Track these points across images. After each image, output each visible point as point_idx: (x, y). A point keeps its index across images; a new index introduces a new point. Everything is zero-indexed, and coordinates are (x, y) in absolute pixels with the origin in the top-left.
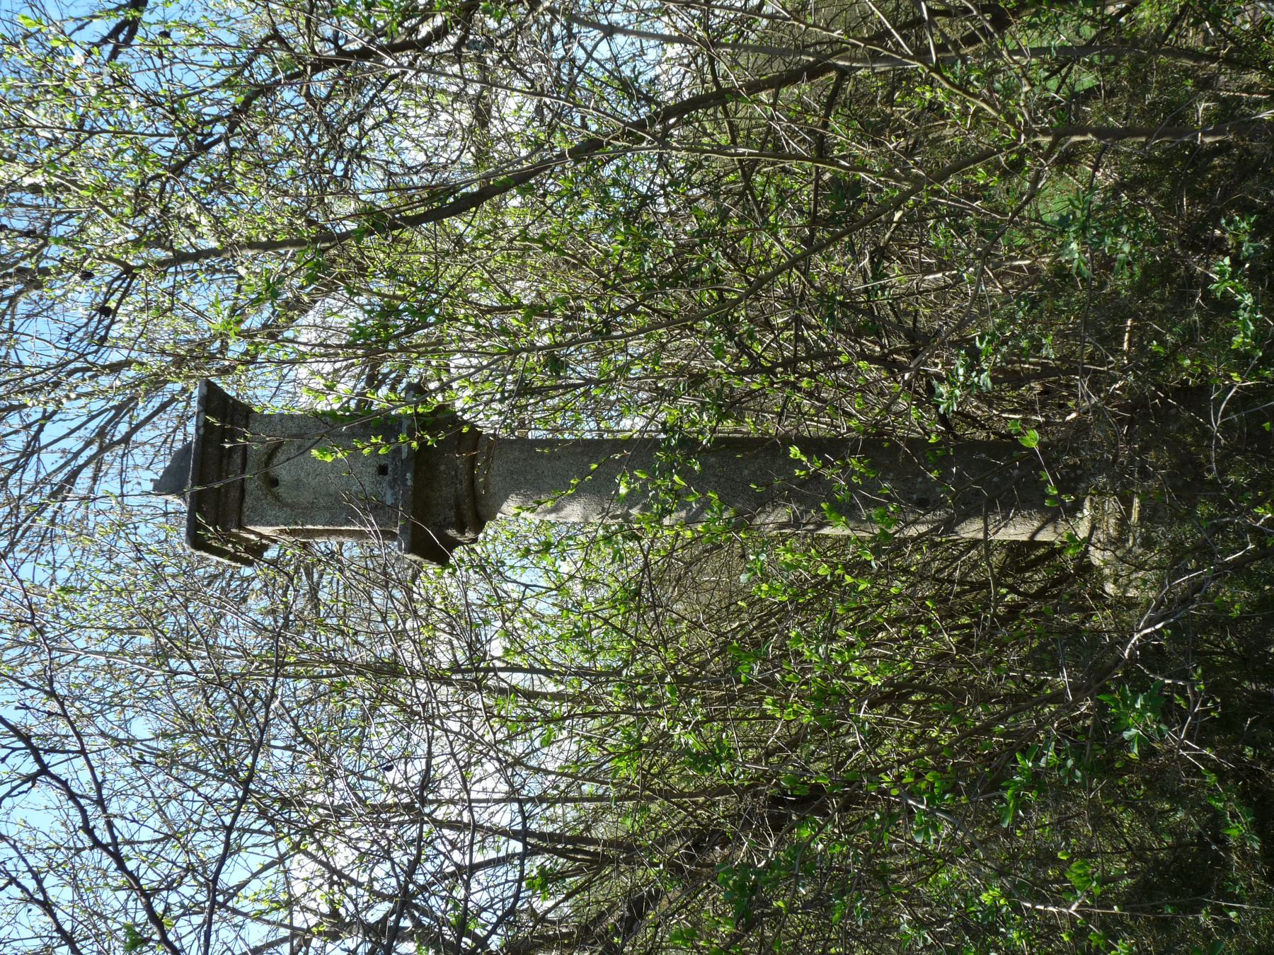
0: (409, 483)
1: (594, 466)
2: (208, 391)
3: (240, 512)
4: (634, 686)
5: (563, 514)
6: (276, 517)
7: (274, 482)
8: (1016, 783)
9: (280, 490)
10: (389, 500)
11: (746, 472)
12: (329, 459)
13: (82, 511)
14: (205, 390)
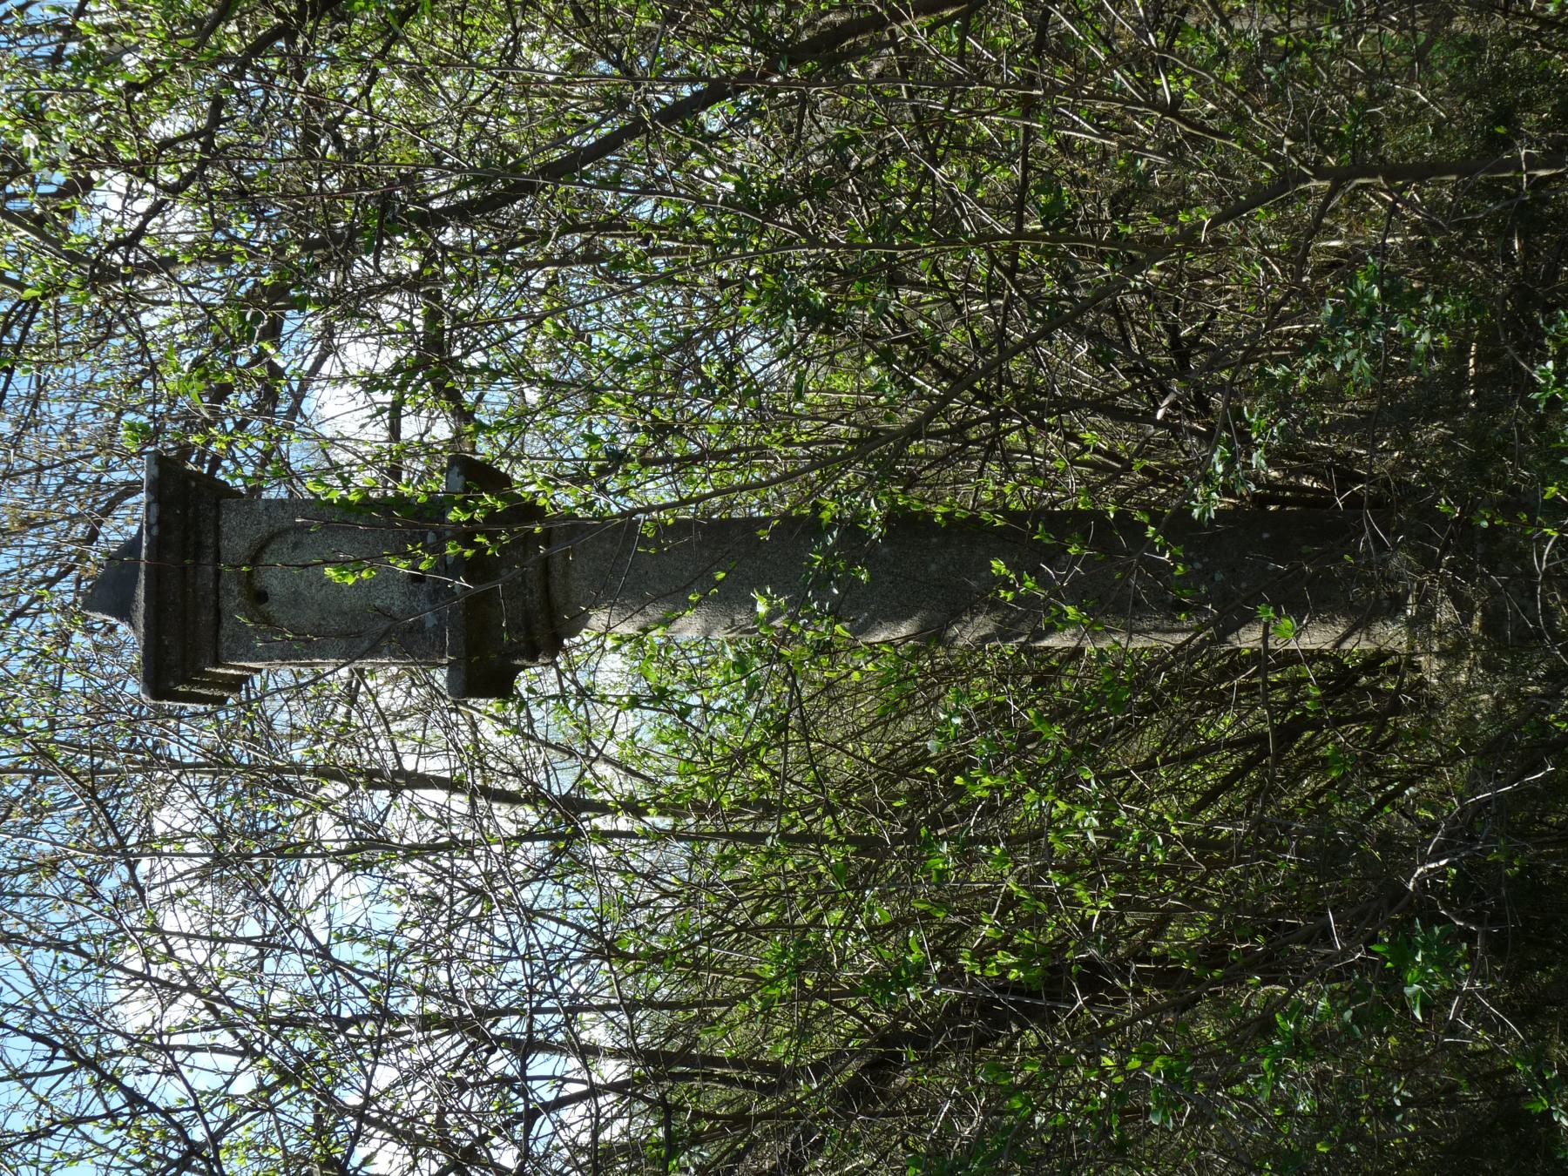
1: (721, 575)
2: (161, 471)
5: (674, 627)
7: (261, 597)
8: (1275, 1049)
9: (271, 608)
10: (430, 620)
11: (933, 567)
12: (350, 581)
13: (283, 1106)
14: (155, 471)
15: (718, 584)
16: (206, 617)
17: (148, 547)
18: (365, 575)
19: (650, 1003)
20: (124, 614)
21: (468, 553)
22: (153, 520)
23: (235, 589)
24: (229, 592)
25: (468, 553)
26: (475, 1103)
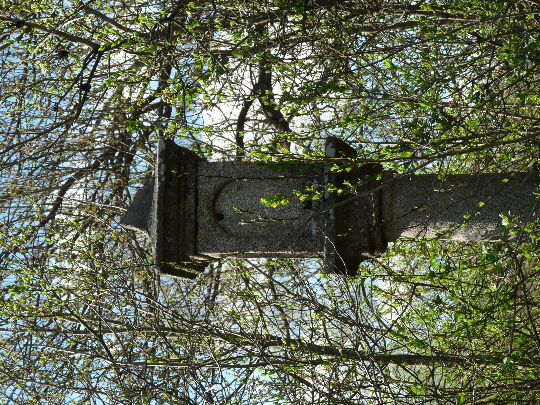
0: (332, 217)
1: (482, 204)
2: (166, 146)
3: (196, 242)
4: (484, 266)
6: (225, 245)
7: (220, 217)
12: (274, 206)
14: (164, 146)
15: (480, 209)
16: (190, 227)
17: (159, 188)
18: (282, 202)
19: (381, 61)
20: (144, 225)
21: (340, 191)
22: (162, 173)
23: (206, 212)
24: (202, 213)
25: (340, 191)
26: (401, 163)
